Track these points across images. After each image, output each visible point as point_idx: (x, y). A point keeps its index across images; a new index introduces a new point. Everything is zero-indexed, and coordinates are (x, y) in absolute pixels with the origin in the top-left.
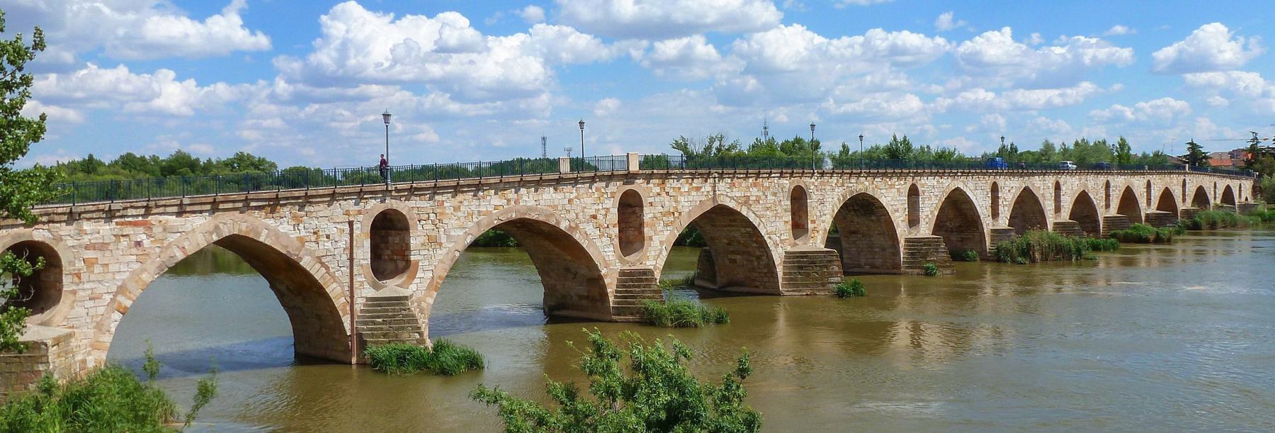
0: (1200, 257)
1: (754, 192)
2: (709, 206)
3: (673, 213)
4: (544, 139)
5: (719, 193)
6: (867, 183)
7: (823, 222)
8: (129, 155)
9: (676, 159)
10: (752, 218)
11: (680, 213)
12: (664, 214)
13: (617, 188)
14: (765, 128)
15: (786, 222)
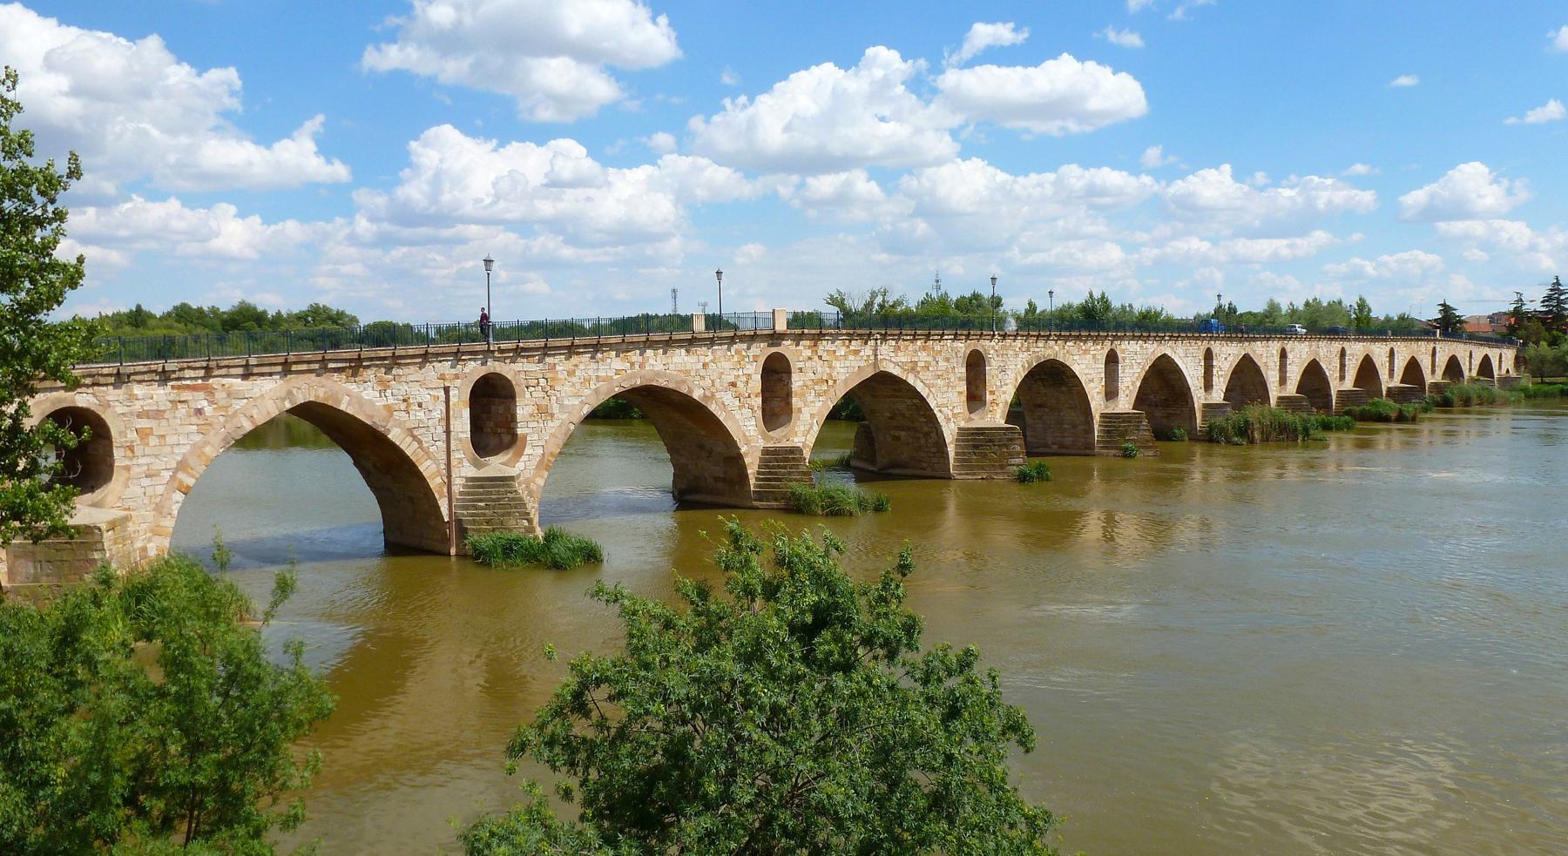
3: (827, 381)
4: (674, 291)
6: (1057, 348)
7: (1004, 393)
11: (835, 381)
14: (937, 281)
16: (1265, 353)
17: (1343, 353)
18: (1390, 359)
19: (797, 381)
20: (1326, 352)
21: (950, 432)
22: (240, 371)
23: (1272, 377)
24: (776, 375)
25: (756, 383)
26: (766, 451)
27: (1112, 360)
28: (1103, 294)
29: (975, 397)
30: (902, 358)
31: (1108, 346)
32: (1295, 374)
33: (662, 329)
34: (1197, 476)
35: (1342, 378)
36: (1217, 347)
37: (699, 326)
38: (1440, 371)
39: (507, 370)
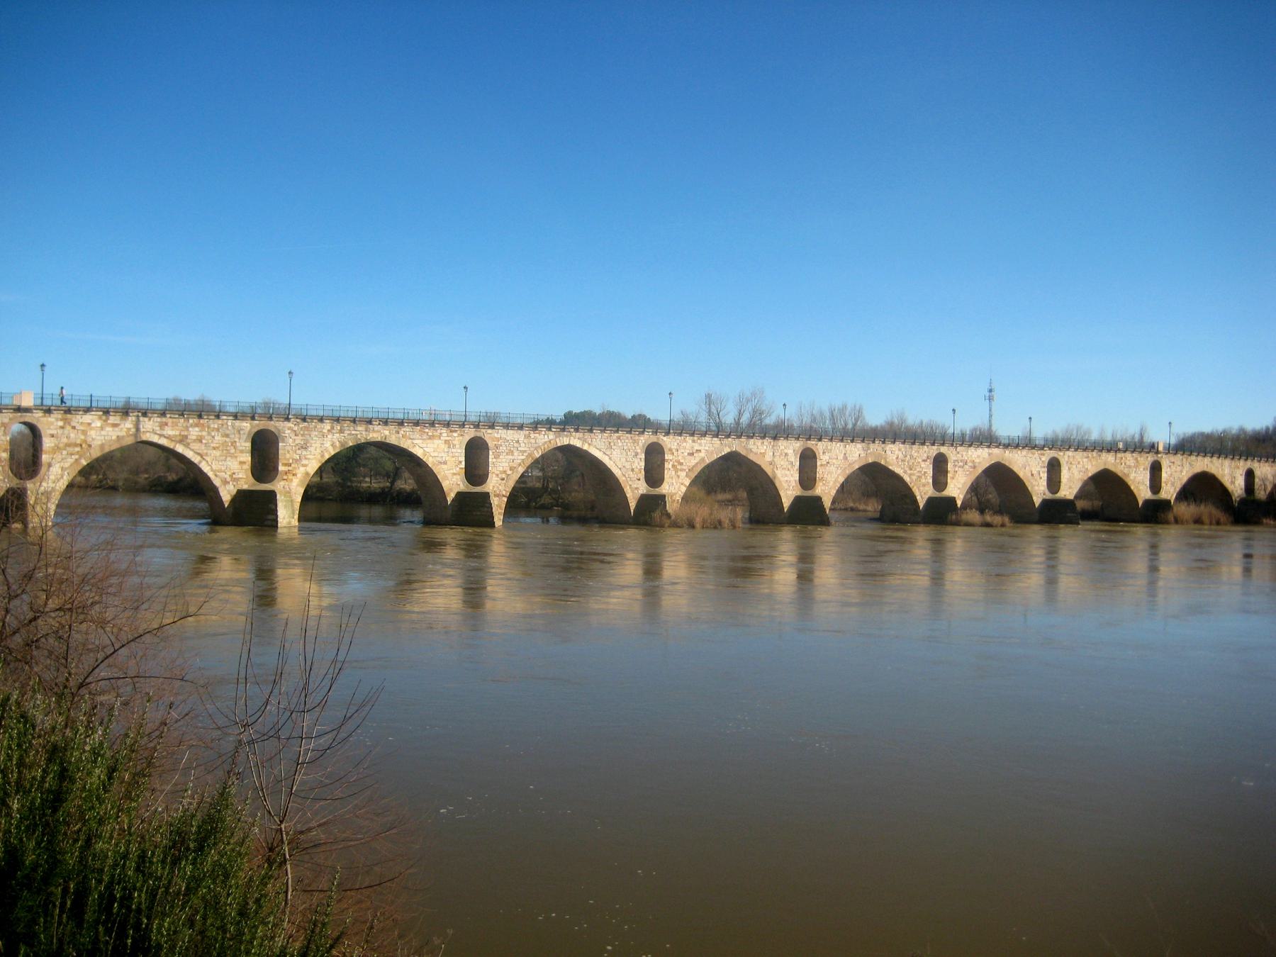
0: (1249, 560)
1: (194, 432)
2: (129, 441)
5: (144, 430)
8: (570, 413)
9: (143, 401)
10: (189, 454)
12: (68, 445)
13: (1150, 458)
15: (242, 463)
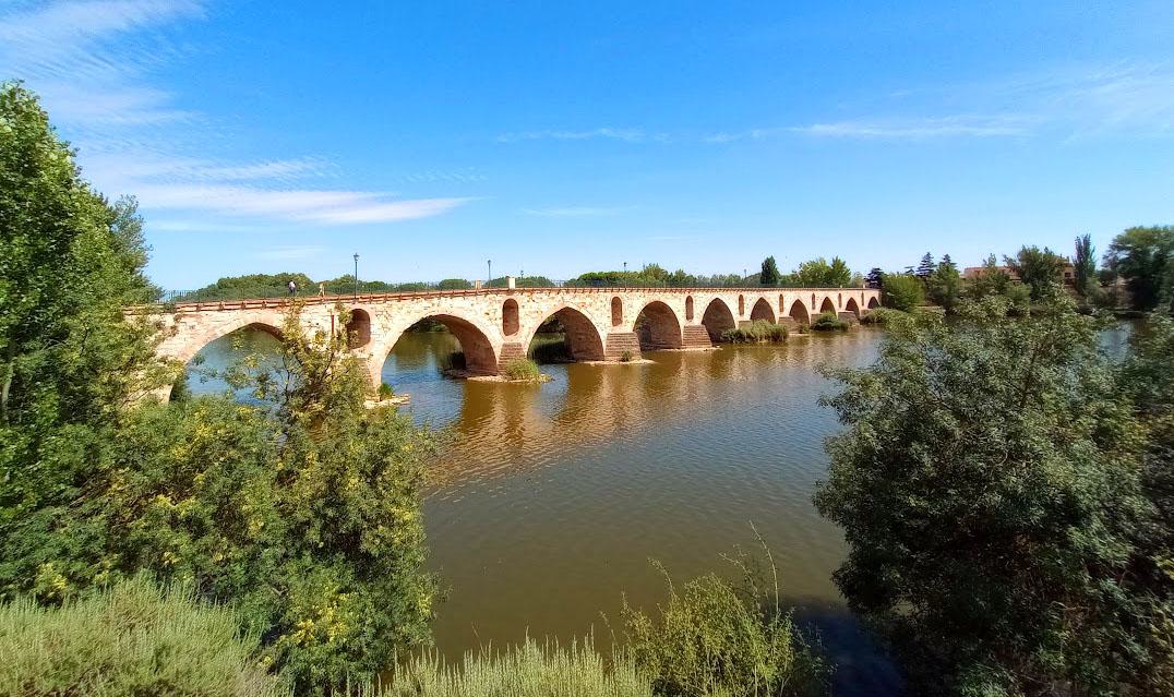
16: (772, 297)
17: (814, 297)
18: (781, 302)
19: (521, 312)
20: (805, 296)
21: (603, 335)
22: (217, 308)
23: (775, 308)
24: (510, 309)
25: (500, 313)
26: (505, 345)
27: (689, 301)
28: (947, 257)
29: (617, 318)
30: (577, 300)
31: (687, 294)
32: (788, 306)
33: (365, 291)
34: (861, 337)
35: (814, 308)
36: (745, 294)
37: (512, 285)
38: (866, 304)
39: (366, 307)
